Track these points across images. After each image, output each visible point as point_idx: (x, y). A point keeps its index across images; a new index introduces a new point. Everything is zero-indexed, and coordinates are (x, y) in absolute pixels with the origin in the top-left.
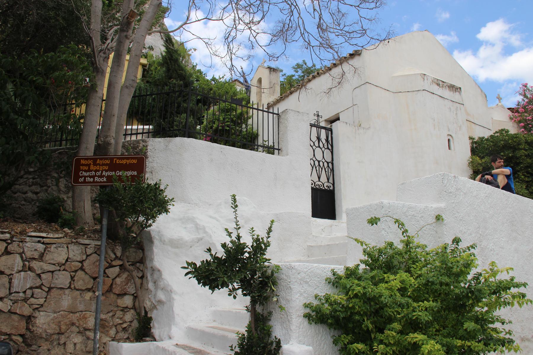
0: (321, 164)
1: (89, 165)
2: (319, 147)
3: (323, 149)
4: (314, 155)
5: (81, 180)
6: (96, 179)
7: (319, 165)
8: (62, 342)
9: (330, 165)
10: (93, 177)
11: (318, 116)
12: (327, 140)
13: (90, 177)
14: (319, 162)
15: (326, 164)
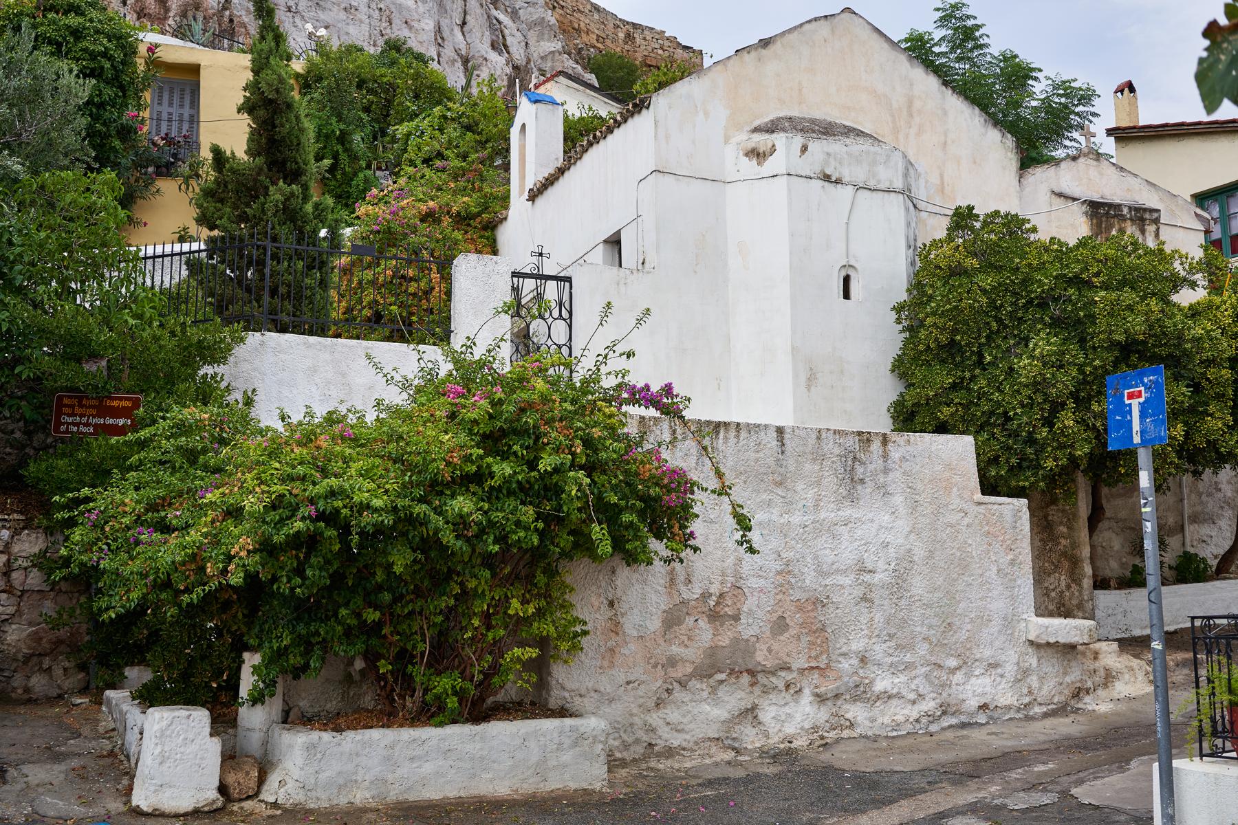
1: (72, 406)
5: (63, 428)
6: (82, 428)
8: (45, 666)
10: (77, 425)
11: (541, 255)
12: (560, 304)
13: (74, 424)
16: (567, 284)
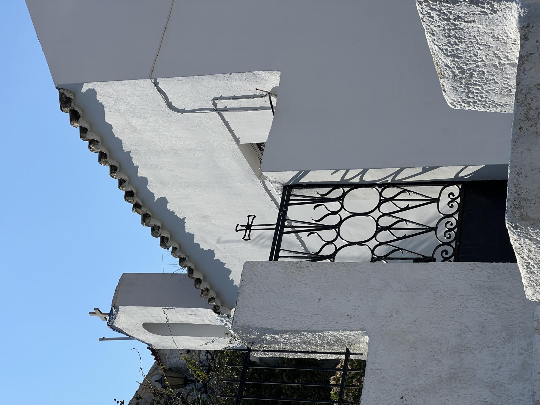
0: (385, 221)
2: (337, 227)
3: (344, 214)
4: (366, 214)
7: (389, 228)
9: (389, 192)
11: (248, 227)
12: (319, 201)
14: (380, 229)
15: (387, 207)
16: (296, 191)
